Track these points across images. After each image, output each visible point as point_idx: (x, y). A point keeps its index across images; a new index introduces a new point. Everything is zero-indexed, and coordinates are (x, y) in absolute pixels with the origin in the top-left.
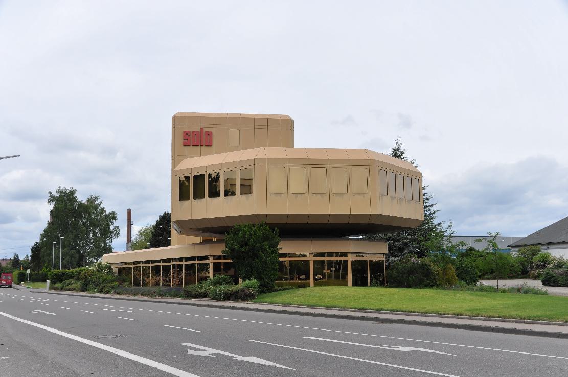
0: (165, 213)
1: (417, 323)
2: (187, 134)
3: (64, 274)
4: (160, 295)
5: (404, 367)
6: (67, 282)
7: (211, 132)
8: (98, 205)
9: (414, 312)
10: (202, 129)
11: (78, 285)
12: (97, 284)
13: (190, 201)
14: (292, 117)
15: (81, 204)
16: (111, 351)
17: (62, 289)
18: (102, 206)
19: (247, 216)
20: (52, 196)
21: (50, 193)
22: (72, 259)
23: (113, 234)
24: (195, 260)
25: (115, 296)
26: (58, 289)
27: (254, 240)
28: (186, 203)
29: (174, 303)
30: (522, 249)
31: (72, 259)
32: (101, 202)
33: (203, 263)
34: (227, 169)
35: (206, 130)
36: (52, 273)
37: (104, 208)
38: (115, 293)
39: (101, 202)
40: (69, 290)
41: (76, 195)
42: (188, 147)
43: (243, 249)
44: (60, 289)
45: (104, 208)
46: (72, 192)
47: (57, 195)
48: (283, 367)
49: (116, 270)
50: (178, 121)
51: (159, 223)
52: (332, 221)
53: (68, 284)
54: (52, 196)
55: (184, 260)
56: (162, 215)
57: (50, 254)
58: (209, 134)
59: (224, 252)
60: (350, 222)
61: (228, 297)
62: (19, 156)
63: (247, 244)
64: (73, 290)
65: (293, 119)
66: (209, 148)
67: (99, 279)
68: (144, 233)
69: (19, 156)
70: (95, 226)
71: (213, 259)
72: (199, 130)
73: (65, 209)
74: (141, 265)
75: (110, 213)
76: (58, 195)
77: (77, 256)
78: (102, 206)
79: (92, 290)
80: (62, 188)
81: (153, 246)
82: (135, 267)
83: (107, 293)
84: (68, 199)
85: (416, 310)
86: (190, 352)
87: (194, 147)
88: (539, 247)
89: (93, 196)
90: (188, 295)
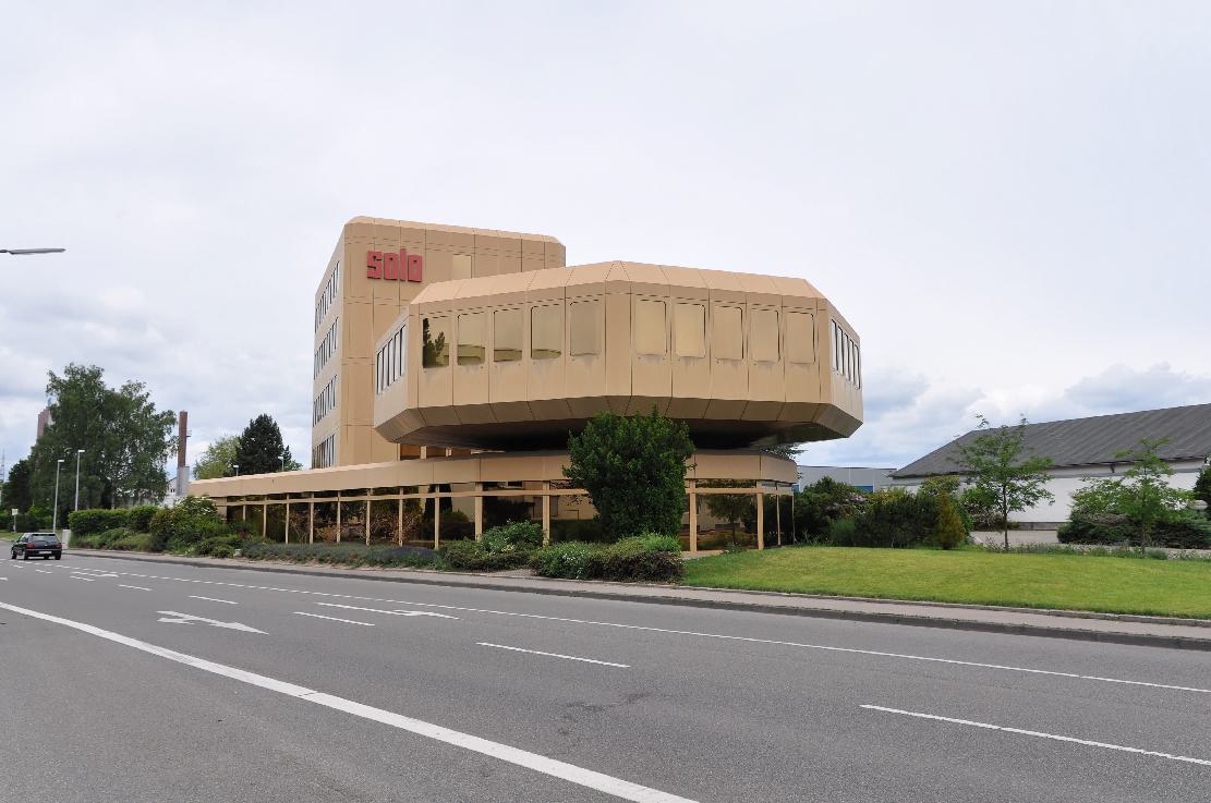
0: (261, 417)
1: (845, 615)
2: (374, 257)
3: (100, 518)
4: (373, 563)
5: (985, 725)
6: (113, 532)
7: (420, 258)
8: (141, 400)
9: (873, 597)
10: (403, 251)
11: (143, 538)
12: (192, 539)
13: (485, 365)
14: (562, 240)
15: (112, 394)
16: (392, 714)
17: (101, 546)
18: (149, 400)
19: (588, 399)
20: (54, 378)
21: (51, 374)
22: (94, 491)
23: (168, 450)
24: (398, 493)
25: (245, 562)
26: (92, 547)
27: (653, 444)
28: (438, 374)
29: (305, 573)
30: (931, 481)
31: (94, 491)
32: (148, 394)
33: (356, 502)
34: (535, 303)
35: (410, 252)
36: (76, 516)
37: (153, 404)
38: (243, 555)
39: (148, 394)
40: (121, 548)
41: (102, 379)
42: (377, 281)
43: (630, 465)
44: (97, 545)
45: (153, 404)
46: (96, 374)
47: (65, 378)
48: (209, 620)
49: (222, 511)
50: (355, 232)
51: (249, 433)
52: (748, 417)
53: (116, 538)
54: (54, 378)
55: (401, 492)
56: (254, 419)
57: (50, 481)
58: (416, 260)
59: (567, 473)
60: (746, 418)
61: (596, 571)
62: (62, 250)
63: (634, 455)
64: (132, 547)
65: (564, 243)
66: (416, 285)
67: (193, 527)
68: (218, 448)
69: (62, 250)
70: (138, 434)
71: (484, 490)
72: (397, 252)
73: (81, 402)
74: (423, 496)
75: (164, 414)
76: (67, 379)
77: (103, 487)
78: (149, 400)
79: (181, 548)
80: (77, 364)
81: (242, 472)
82: (317, 505)
83: (224, 555)
84: (86, 386)
85: (1126, 606)
86: (163, 620)
87: (411, 284)
88: (956, 478)
89: (134, 381)
90: (458, 565)
